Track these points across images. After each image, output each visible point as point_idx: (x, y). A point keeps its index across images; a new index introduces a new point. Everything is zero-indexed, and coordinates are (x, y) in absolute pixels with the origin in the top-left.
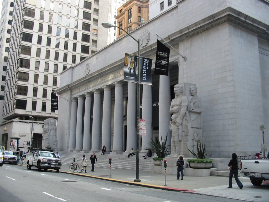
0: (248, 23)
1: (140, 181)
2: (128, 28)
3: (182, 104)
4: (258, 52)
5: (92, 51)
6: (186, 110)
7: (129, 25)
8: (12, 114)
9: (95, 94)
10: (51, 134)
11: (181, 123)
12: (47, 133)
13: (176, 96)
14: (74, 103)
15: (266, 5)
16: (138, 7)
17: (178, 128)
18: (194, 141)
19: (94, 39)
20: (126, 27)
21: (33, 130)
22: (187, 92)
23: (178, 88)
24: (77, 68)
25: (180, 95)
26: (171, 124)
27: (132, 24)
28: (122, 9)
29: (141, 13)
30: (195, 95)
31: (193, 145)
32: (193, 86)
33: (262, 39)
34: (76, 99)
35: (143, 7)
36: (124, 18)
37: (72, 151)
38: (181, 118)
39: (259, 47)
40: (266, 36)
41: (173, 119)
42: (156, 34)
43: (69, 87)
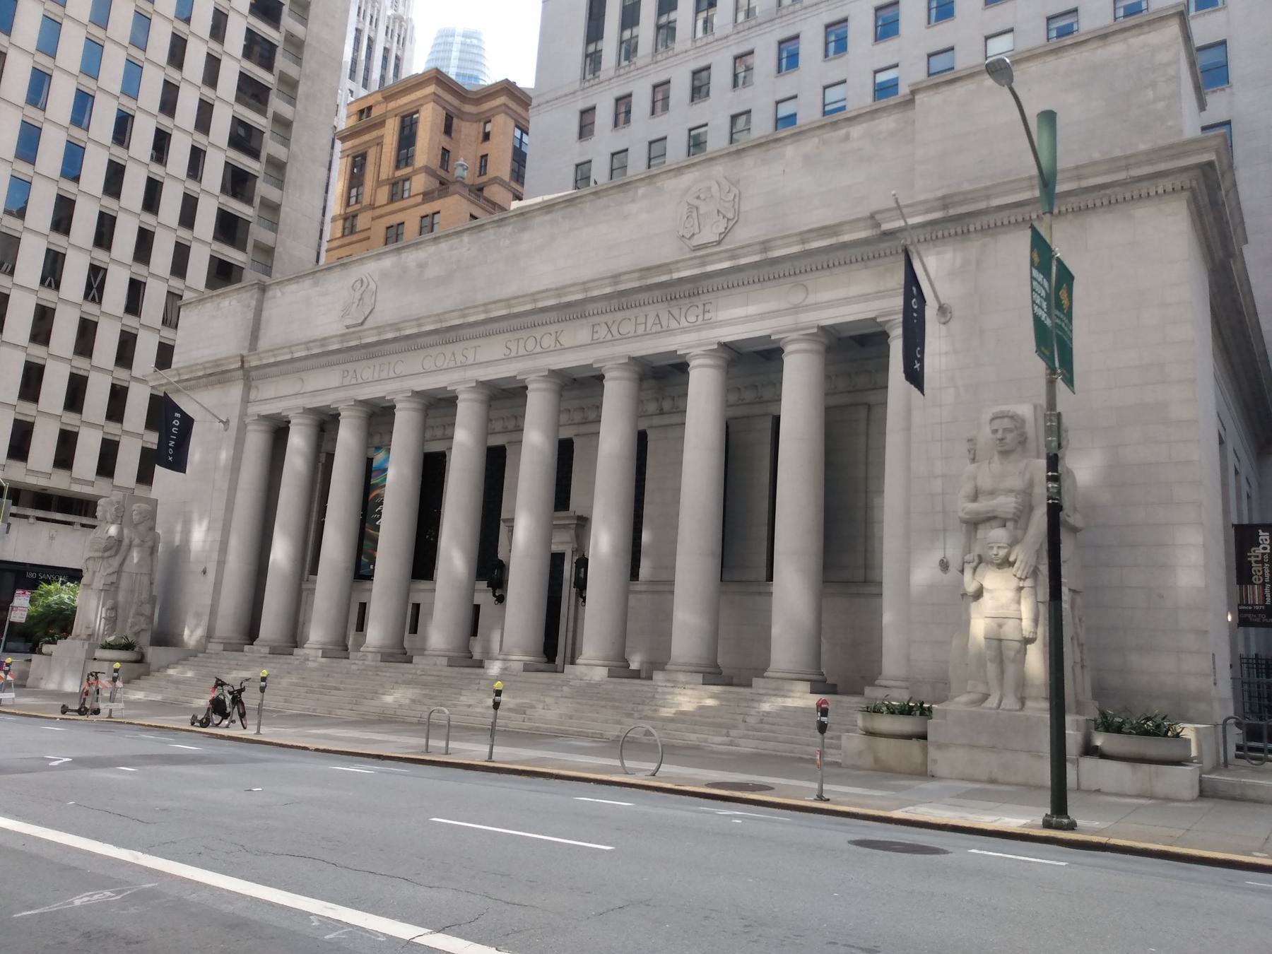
1: (1072, 827)
7: (399, 173)
9: (400, 410)
16: (444, 112)
20: (388, 179)
27: (415, 172)
28: (370, 108)
34: (279, 432)
35: (462, 116)
36: (379, 143)
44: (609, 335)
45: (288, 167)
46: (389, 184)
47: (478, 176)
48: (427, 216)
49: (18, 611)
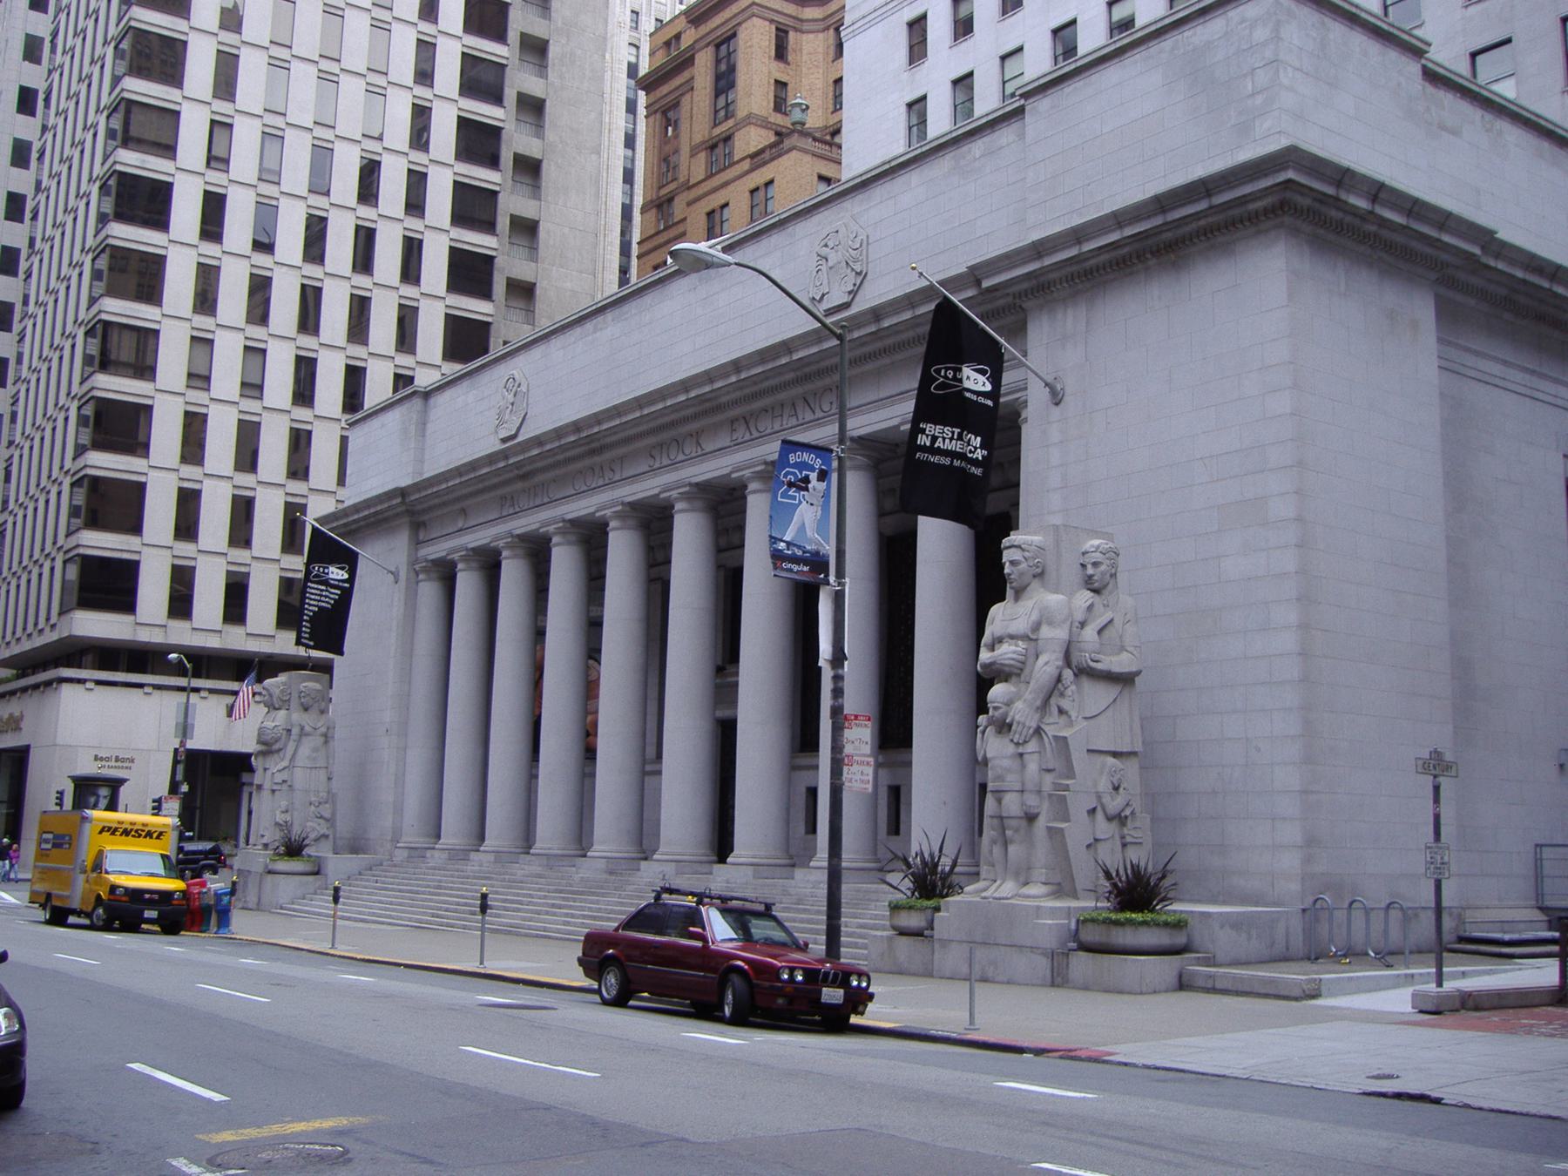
0: (1384, 223)
2: (713, 147)
3: (1046, 632)
4: (1435, 363)
5: (508, 278)
6: (1060, 663)
7: (717, 131)
8: (51, 637)
10: (300, 761)
11: (1034, 725)
12: (281, 754)
13: (1009, 593)
14: (429, 591)
15: (1486, 114)
16: (773, 27)
17: (1021, 750)
18: (1100, 815)
19: (524, 215)
21: (188, 735)
22: (1071, 574)
23: (1023, 550)
24: (448, 394)
25: (1032, 584)
26: (983, 732)
27: (739, 126)
29: (789, 64)
30: (1110, 586)
31: (1092, 840)
32: (1096, 542)
33: (1459, 297)
35: (800, 25)
37: (417, 853)
38: (1038, 703)
39: (1440, 340)
40: (1475, 281)
41: (996, 708)
42: (914, 268)
43: (407, 500)
44: (699, 450)
45: (545, 165)
46: (706, 149)
47: (833, 113)
48: (757, 189)
49: (855, 765)
